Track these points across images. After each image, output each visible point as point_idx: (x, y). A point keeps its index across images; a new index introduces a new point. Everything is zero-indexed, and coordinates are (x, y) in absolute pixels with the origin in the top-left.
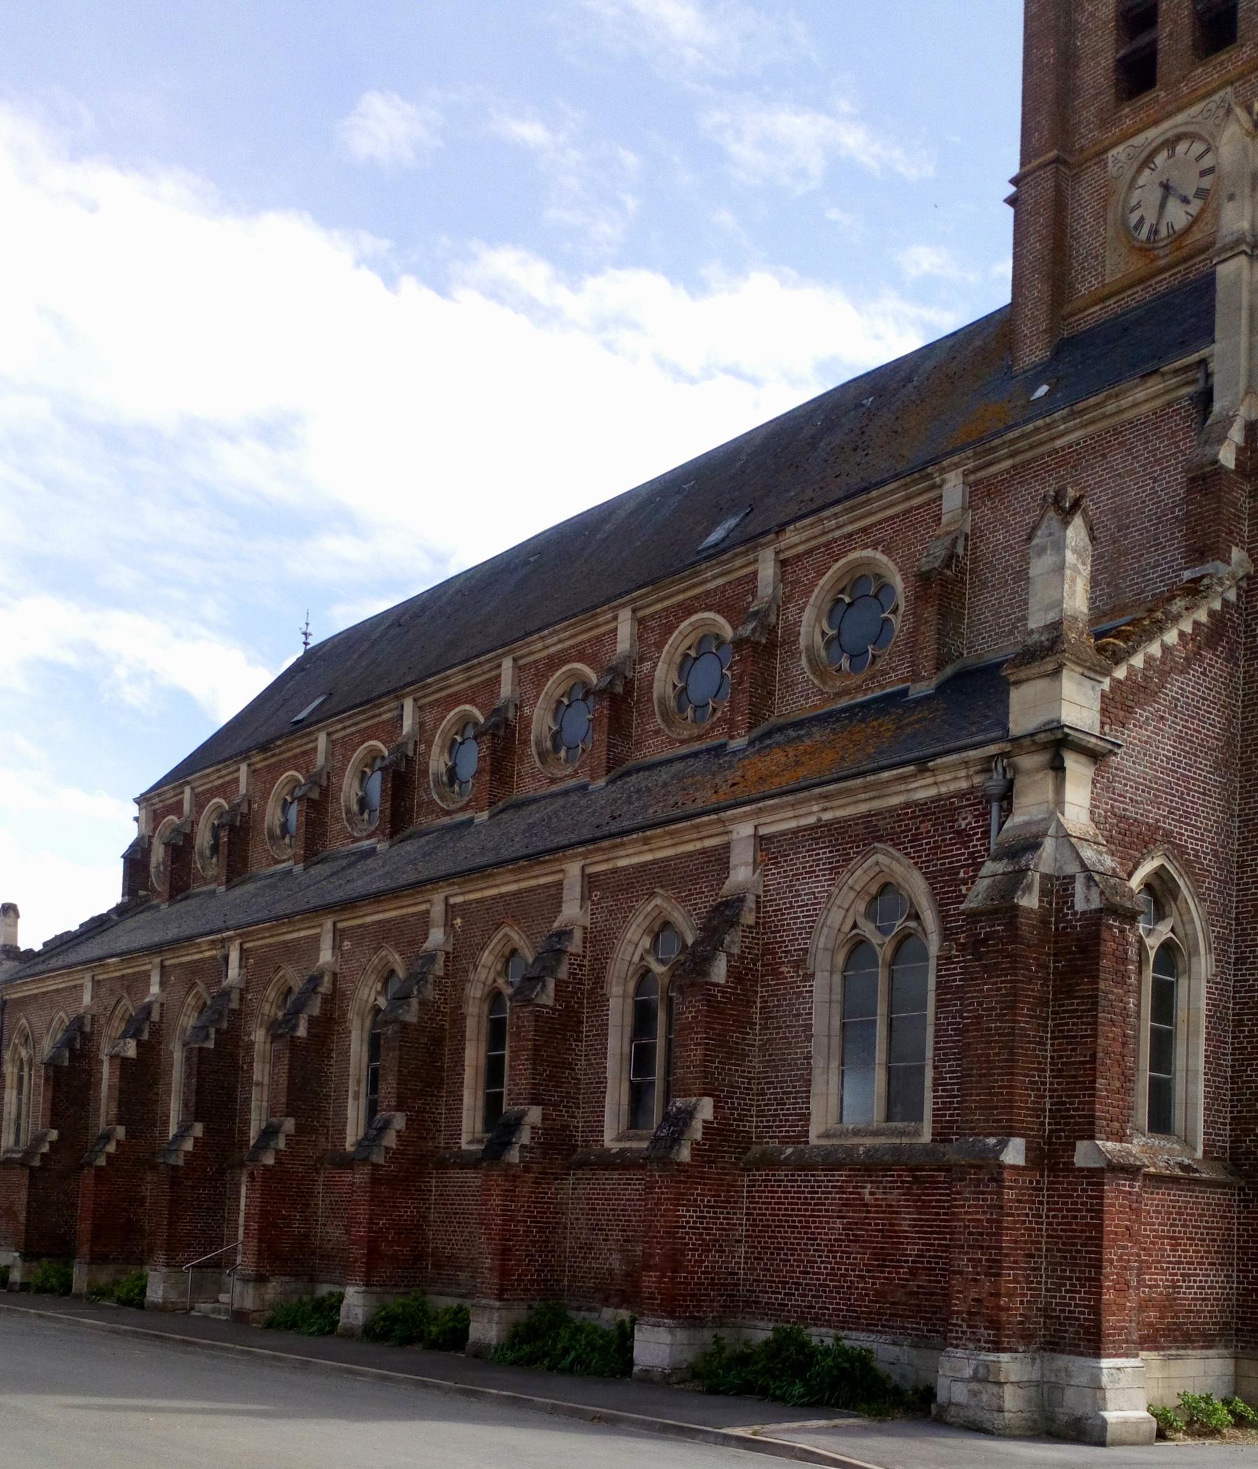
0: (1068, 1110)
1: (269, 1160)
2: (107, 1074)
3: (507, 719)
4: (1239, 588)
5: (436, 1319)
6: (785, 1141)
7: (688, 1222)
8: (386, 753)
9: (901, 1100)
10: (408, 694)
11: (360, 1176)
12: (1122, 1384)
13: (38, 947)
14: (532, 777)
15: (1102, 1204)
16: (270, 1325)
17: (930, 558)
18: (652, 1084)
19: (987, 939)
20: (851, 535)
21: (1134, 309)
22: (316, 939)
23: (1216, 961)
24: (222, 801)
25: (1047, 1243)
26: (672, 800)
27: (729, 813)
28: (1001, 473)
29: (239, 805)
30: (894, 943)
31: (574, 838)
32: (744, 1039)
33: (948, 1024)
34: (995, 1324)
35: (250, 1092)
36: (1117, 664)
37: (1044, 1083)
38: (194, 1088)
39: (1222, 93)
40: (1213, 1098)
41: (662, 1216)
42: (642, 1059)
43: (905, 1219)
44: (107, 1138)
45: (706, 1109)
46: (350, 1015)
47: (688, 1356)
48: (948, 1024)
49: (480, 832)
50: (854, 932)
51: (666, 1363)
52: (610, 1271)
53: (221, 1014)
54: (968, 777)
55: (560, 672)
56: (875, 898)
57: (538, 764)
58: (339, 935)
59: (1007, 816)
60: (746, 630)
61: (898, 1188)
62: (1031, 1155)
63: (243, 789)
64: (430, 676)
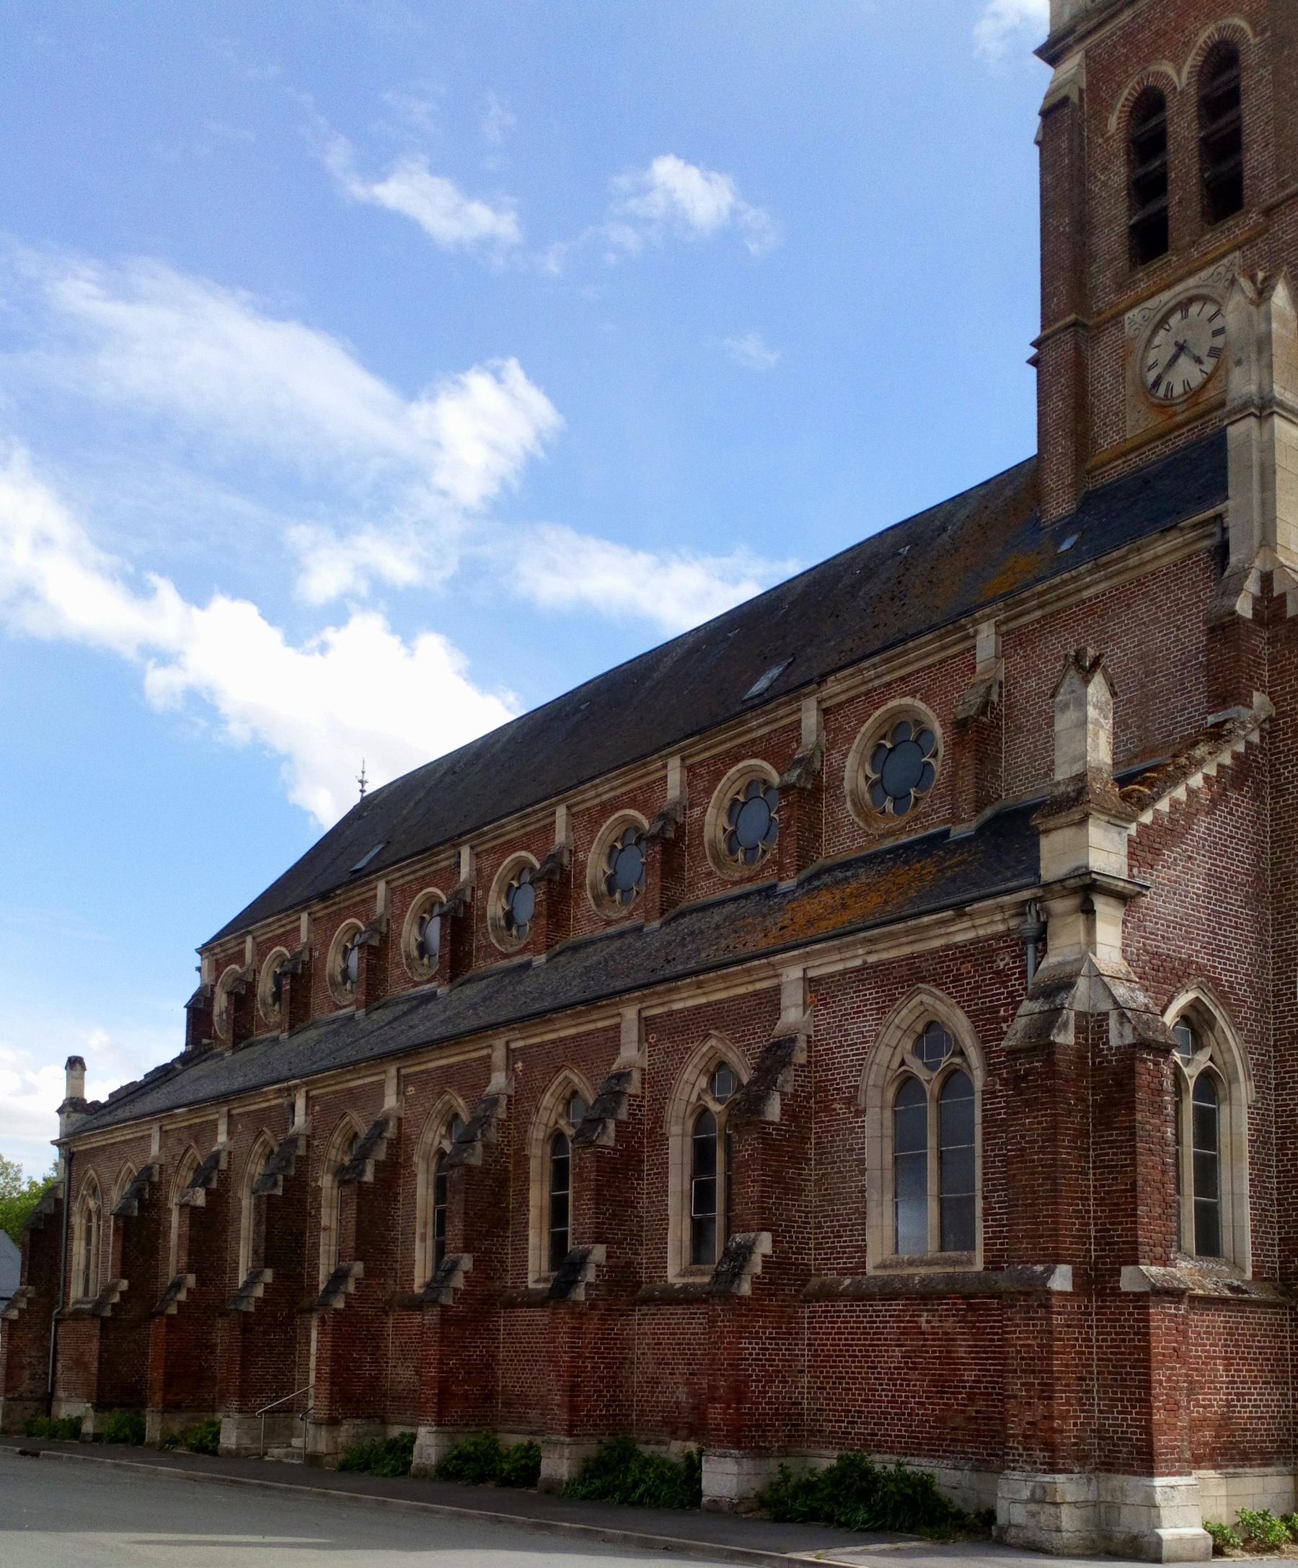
0: (1112, 1237)
1: (339, 1304)
2: (175, 1222)
3: (562, 865)
4: (1262, 730)
5: (508, 1456)
6: (843, 1272)
7: (751, 1354)
8: (445, 899)
9: (954, 1228)
10: (465, 843)
11: (430, 1317)
12: (1177, 1501)
13: (104, 1099)
14: (588, 918)
15: (1148, 1327)
16: (344, 1468)
17: (966, 706)
18: (713, 1220)
19: (1029, 1073)
20: (889, 684)
21: (1154, 463)
22: (381, 1085)
23: (1256, 1087)
24: (283, 949)
25: (1098, 1366)
26: (724, 943)
27: (778, 957)
28: (1032, 623)
29: (301, 953)
30: (941, 1079)
31: (629, 982)
32: (800, 1174)
33: (996, 1156)
34: (1050, 1446)
35: (318, 1237)
36: (1142, 810)
37: (1088, 1212)
38: (263, 1234)
39: (1231, 257)
40: (1260, 1220)
41: (725, 1349)
42: (703, 1196)
43: (961, 1346)
44: (177, 1286)
45: (765, 1244)
46: (415, 1159)
47: (757, 1484)
48: (996, 1156)
49: (538, 975)
50: (903, 1068)
51: (733, 1493)
52: (677, 1403)
53: (288, 1162)
54: (1004, 920)
55: (613, 818)
56: (921, 1036)
57: (594, 907)
58: (403, 1081)
59: (1042, 957)
60: (793, 776)
61: (953, 1315)
62: (1079, 1281)
63: (304, 938)
64: (486, 824)
